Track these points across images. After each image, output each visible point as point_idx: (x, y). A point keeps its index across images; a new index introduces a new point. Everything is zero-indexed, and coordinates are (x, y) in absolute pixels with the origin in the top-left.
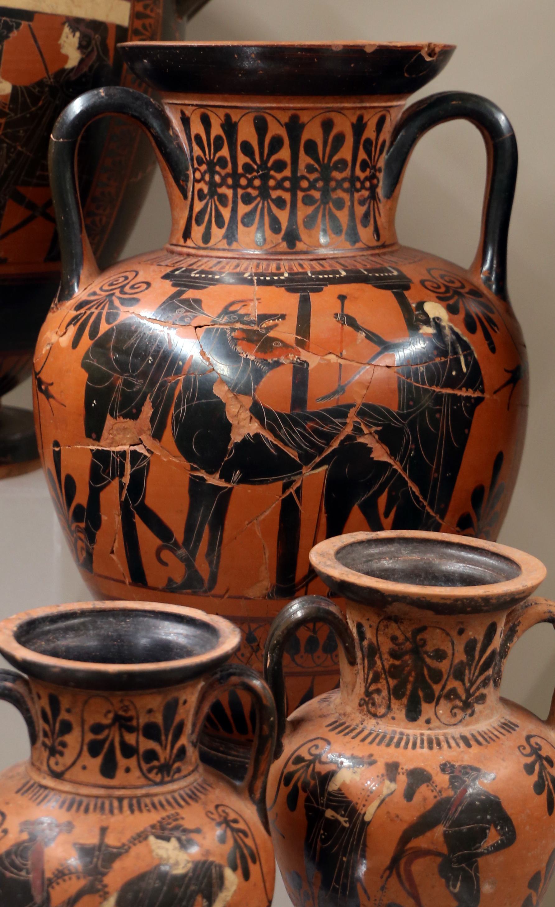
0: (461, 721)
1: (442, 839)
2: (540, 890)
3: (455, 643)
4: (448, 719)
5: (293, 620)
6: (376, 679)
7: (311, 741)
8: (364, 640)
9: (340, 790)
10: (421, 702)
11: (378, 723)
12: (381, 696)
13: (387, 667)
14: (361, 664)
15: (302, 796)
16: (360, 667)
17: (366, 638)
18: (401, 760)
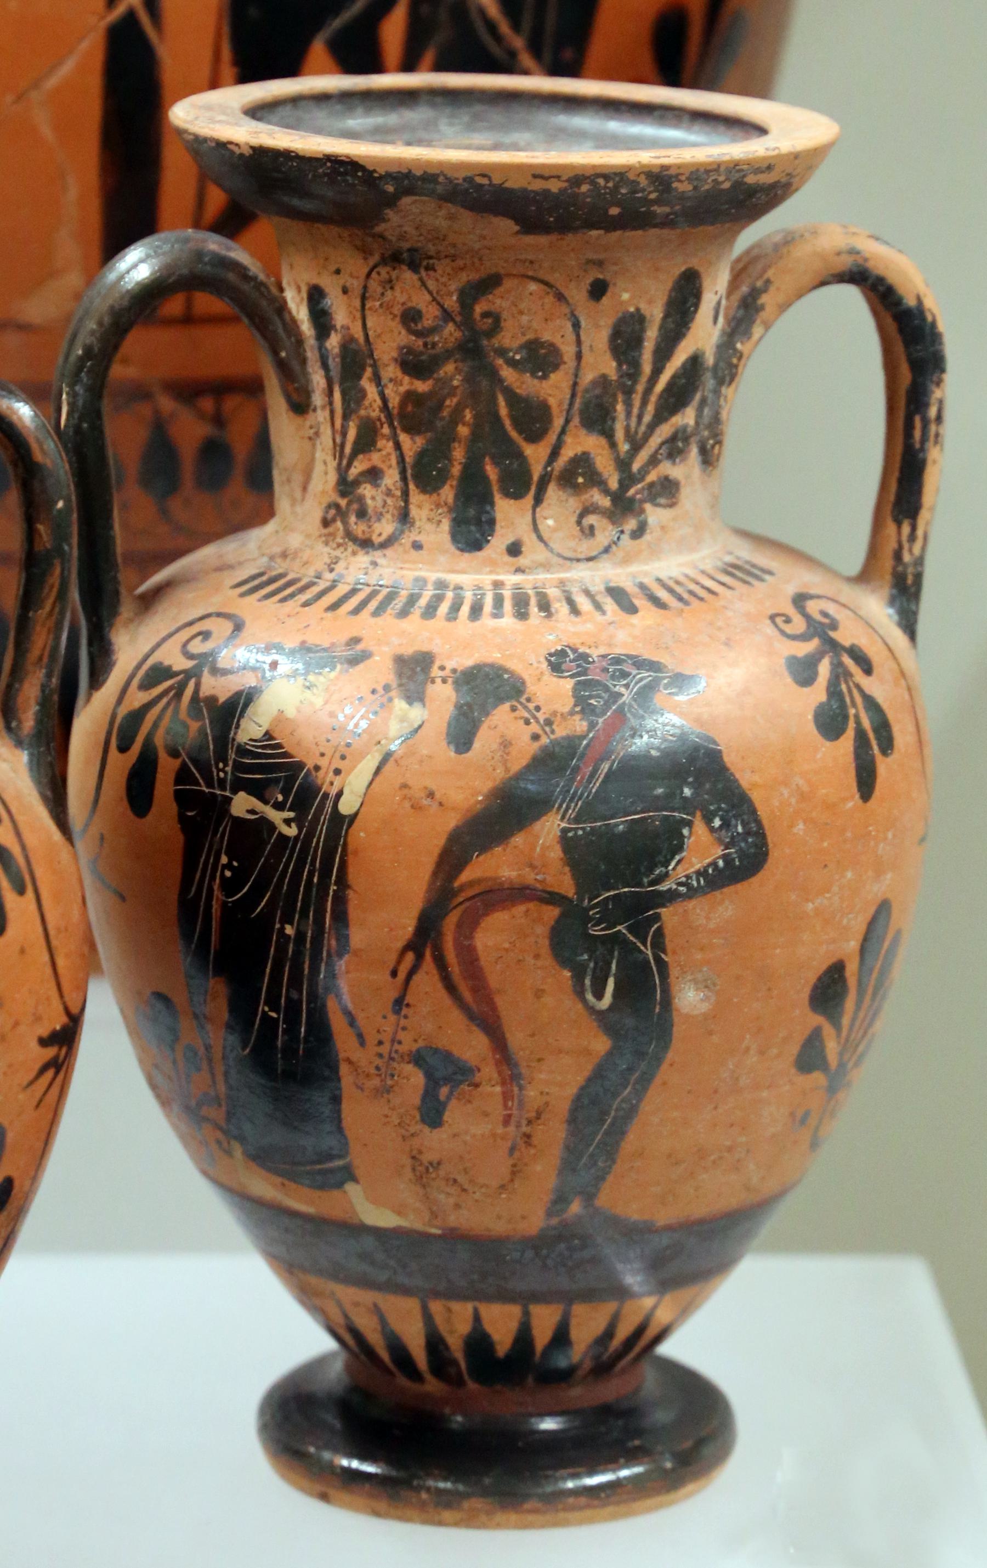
0: (607, 550)
1: (556, 853)
2: (846, 1021)
3: (583, 324)
4: (572, 544)
5: (124, 290)
6: (366, 442)
7: (191, 624)
8: (328, 336)
9: (268, 735)
10: (492, 496)
11: (375, 564)
12: (383, 488)
13: (394, 402)
14: (323, 407)
15: (167, 768)
16: (322, 416)
17: (333, 327)
18: (436, 646)
